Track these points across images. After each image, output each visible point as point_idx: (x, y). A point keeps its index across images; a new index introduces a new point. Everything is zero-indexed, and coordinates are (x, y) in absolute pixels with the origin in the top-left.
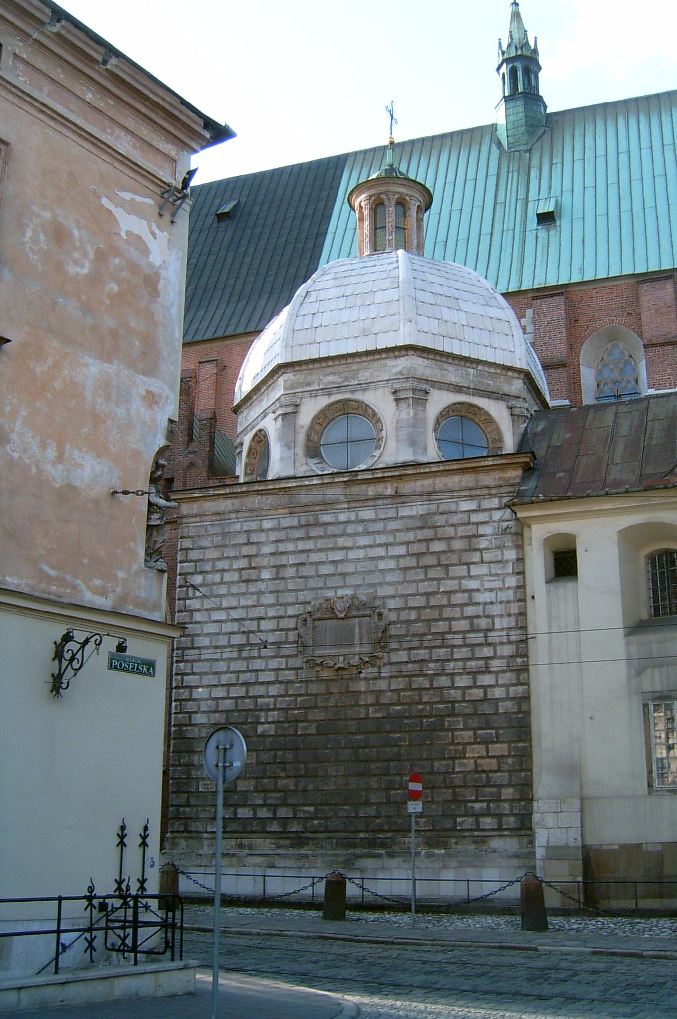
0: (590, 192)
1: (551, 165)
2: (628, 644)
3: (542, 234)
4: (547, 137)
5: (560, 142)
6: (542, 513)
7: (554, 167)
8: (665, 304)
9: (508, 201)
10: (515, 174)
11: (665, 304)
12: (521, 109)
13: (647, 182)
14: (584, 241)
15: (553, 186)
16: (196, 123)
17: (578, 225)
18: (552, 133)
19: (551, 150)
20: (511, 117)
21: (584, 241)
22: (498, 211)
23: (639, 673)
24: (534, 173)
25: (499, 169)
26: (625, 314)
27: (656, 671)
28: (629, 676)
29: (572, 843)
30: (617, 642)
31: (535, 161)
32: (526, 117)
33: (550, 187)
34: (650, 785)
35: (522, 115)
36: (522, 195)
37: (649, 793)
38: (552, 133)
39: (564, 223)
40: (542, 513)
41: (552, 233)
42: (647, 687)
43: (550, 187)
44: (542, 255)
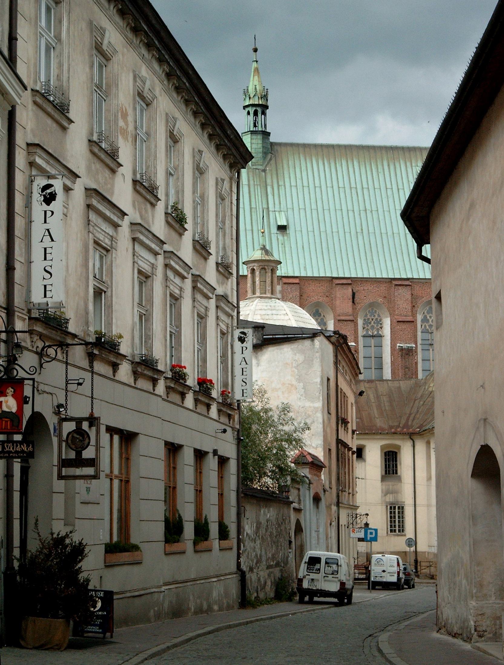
0: (302, 212)
1: (279, 186)
2: (382, 485)
3: (280, 237)
4: (273, 162)
5: (281, 170)
6: (362, 437)
7: (280, 187)
8: (348, 297)
9: (257, 206)
10: (259, 187)
11: (348, 297)
12: (260, 142)
13: (333, 212)
14: (303, 247)
15: (281, 202)
16: (161, 192)
17: (299, 235)
18: (275, 158)
19: (277, 170)
20: (254, 145)
21: (303, 247)
22: (253, 214)
23: (385, 495)
24: (269, 189)
25: (249, 181)
26: (325, 296)
27: (391, 495)
28: (382, 497)
29: (363, 551)
30: (378, 483)
31: (269, 181)
32: (263, 147)
33: (280, 203)
34: (387, 533)
35: (260, 146)
36: (265, 206)
37: (387, 535)
38: (275, 158)
39: (291, 230)
40: (362, 437)
41: (285, 238)
42: (388, 500)
43: (280, 203)
44: (283, 253)
